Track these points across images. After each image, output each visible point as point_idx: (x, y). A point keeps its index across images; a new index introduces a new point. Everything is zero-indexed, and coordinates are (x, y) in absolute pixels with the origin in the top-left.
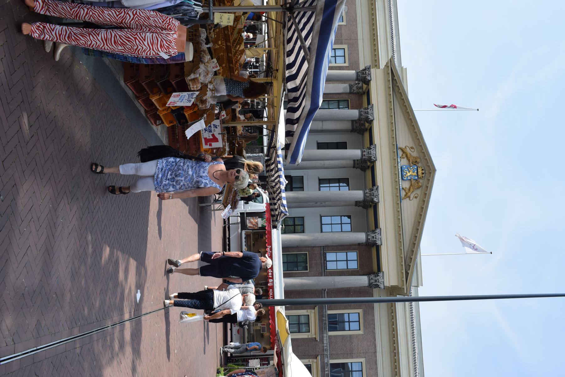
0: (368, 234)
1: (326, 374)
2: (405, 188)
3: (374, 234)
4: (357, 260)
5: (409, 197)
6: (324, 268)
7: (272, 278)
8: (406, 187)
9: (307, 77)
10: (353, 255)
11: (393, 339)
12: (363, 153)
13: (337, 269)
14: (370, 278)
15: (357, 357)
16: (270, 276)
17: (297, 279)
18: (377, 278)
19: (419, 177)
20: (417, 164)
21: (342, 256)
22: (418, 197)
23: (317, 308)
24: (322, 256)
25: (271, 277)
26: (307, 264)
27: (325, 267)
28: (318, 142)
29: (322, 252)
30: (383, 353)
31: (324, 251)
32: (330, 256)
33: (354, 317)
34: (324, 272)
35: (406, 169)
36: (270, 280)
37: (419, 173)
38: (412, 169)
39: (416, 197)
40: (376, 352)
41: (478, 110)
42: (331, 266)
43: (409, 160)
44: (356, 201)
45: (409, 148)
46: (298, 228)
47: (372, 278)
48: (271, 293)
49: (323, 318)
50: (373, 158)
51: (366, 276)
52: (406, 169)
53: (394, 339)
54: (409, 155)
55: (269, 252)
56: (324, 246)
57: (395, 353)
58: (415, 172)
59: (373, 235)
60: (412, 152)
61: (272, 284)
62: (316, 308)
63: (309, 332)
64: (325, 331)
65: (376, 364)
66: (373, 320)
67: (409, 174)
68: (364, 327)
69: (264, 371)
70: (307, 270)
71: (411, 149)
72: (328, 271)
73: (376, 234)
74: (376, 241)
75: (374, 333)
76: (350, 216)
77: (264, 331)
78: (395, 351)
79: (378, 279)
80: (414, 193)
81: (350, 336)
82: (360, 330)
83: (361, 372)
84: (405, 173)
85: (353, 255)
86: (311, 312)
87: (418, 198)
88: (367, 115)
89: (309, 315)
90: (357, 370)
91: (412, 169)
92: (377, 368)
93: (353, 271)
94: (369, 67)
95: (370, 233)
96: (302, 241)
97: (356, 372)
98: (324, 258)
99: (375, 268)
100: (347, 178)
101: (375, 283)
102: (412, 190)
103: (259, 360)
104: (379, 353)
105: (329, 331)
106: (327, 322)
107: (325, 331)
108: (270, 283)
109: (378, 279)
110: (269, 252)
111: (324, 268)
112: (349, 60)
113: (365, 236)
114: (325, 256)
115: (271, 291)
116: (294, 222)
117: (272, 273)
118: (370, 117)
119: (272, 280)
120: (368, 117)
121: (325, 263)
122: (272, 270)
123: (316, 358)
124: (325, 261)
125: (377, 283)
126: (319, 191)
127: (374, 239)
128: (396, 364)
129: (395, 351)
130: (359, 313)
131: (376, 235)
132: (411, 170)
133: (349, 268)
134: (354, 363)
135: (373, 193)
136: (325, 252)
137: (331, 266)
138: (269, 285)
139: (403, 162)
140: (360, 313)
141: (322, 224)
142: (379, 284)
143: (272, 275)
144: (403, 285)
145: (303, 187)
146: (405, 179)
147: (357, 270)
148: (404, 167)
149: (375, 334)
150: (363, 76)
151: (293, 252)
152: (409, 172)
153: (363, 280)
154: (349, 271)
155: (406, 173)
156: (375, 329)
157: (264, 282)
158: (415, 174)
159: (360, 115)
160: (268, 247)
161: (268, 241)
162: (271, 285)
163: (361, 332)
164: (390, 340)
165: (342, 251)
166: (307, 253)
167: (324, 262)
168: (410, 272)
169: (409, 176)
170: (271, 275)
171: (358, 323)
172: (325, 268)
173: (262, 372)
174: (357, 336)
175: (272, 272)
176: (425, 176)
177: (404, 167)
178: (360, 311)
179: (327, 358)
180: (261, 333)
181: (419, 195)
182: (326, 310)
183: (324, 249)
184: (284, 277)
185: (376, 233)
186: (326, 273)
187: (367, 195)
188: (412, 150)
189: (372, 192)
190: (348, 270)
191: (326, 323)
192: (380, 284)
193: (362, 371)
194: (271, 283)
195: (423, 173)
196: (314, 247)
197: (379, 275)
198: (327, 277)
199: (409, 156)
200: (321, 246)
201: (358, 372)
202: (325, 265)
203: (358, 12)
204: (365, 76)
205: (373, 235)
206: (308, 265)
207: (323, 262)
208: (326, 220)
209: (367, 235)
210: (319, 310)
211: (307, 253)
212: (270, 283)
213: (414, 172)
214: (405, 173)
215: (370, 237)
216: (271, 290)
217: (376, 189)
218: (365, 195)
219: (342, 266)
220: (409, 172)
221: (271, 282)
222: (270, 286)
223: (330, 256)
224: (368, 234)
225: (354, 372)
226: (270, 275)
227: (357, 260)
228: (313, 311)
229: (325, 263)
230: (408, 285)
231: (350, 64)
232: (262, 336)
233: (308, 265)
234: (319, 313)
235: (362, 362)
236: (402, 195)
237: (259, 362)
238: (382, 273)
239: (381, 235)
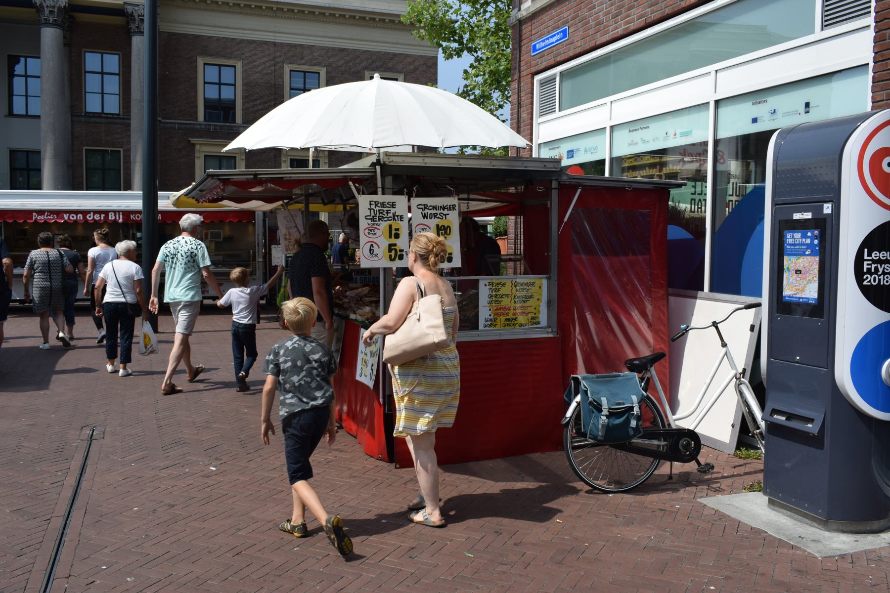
0: (43, 21)
3: (44, 9)
4: (102, 54)
6: (116, 118)
7: (106, 213)
10: (92, 61)
11: (242, 8)
12: (51, 22)
13: (119, 95)
15: (282, 78)
16: (102, 218)
17: (134, 171)
18: (136, 17)
21: (92, 83)
23: (193, 140)
24: (93, 120)
25: (103, 216)
26: (108, 150)
27: (115, 116)
28: (7, 114)
29: (83, 119)
30: (277, 31)
31: (82, 116)
32: (93, 104)
33: (212, 74)
34: (123, 119)
36: (111, 217)
40: (274, 44)
42: (113, 106)
44: (64, 46)
47: (137, 27)
48: (138, 217)
49: (212, 130)
51: (133, 37)
53: (317, 13)
55: (47, 216)
56: (72, 115)
57: (277, 8)
59: (47, 12)
61: (119, 214)
62: (192, 142)
64: (234, 129)
65: (295, 46)
66: (218, 39)
68: (230, 57)
69: (285, 235)
70: (120, 151)
72: (123, 111)
73: (45, 5)
75: (241, 42)
76: (9, 56)
77: (217, 235)
78: (275, 9)
79: (139, 16)
81: (245, 85)
82: (235, 67)
83: (307, 74)
85: (92, 61)
86: (199, 151)
89: (205, 156)
90: (303, 80)
92: (302, 46)
93: (123, 63)
95: (43, 18)
96: (56, 156)
97: (303, 83)
98: (96, 117)
99: (118, 20)
100: (8, 59)
103: (273, 246)
104: (277, 38)
105: (234, 121)
106: (218, 124)
107: (234, 129)
108: (117, 219)
109: (139, 16)
110: (47, 216)
111: (116, 118)
113: (48, 28)
114: (91, 115)
115: (135, 217)
116: (21, 170)
117: (96, 212)
119: (110, 214)
121: (106, 116)
122: (88, 212)
123: (193, 144)
124: (103, 115)
126: (42, 118)
127: (56, 10)
128: (377, 20)
129: (275, 9)
130: (205, 64)
131: (47, 6)
133: (117, 72)
134: (292, 85)
136: (83, 114)
137: (113, 106)
138: (121, 221)
140: (205, 62)
141: (27, 116)
143: (76, 212)
145: (26, 151)
147: (86, 50)
149: (243, 40)
151: (83, 175)
153: (140, 44)
154: (123, 71)
156: (234, 39)
157: (123, 232)
159: (47, 23)
160: (36, 218)
161: (20, 219)
162: (121, 216)
163: (239, 65)
164: (357, 25)
165: (82, 80)
166: (86, 149)
167: (105, 117)
170: (98, 215)
171: (222, 67)
172: (117, 116)
173: (286, 239)
174: (245, 73)
175: (92, 213)
178: (200, 62)
180: (222, 240)
182: (196, 122)
183: (78, 116)
184: (40, 189)
186: (125, 117)
190: (121, 75)
191: (221, 126)
193: (305, 72)
194: (117, 216)
196: (73, 135)
197: (130, 11)
198: (132, 114)
200: (72, 121)
201: (307, 80)
202: (111, 116)
203: (332, 43)
205: (47, 12)
206: (109, 149)
207: (103, 120)
208: (19, 107)
209: (47, 24)
210: (197, 137)
211: (86, 149)
212: (117, 219)
215: (51, 19)
216: (132, 217)
219: (113, 85)
221: (115, 216)
222: (123, 219)
223: (93, 104)
224: (43, 21)
225: (306, 86)
226: (100, 217)
227: (102, 54)
228: (197, 147)
229: (106, 116)
232: (229, 239)
233: (109, 149)
234: (201, 137)
235: (291, 71)
237: (276, 246)
238: (126, 6)
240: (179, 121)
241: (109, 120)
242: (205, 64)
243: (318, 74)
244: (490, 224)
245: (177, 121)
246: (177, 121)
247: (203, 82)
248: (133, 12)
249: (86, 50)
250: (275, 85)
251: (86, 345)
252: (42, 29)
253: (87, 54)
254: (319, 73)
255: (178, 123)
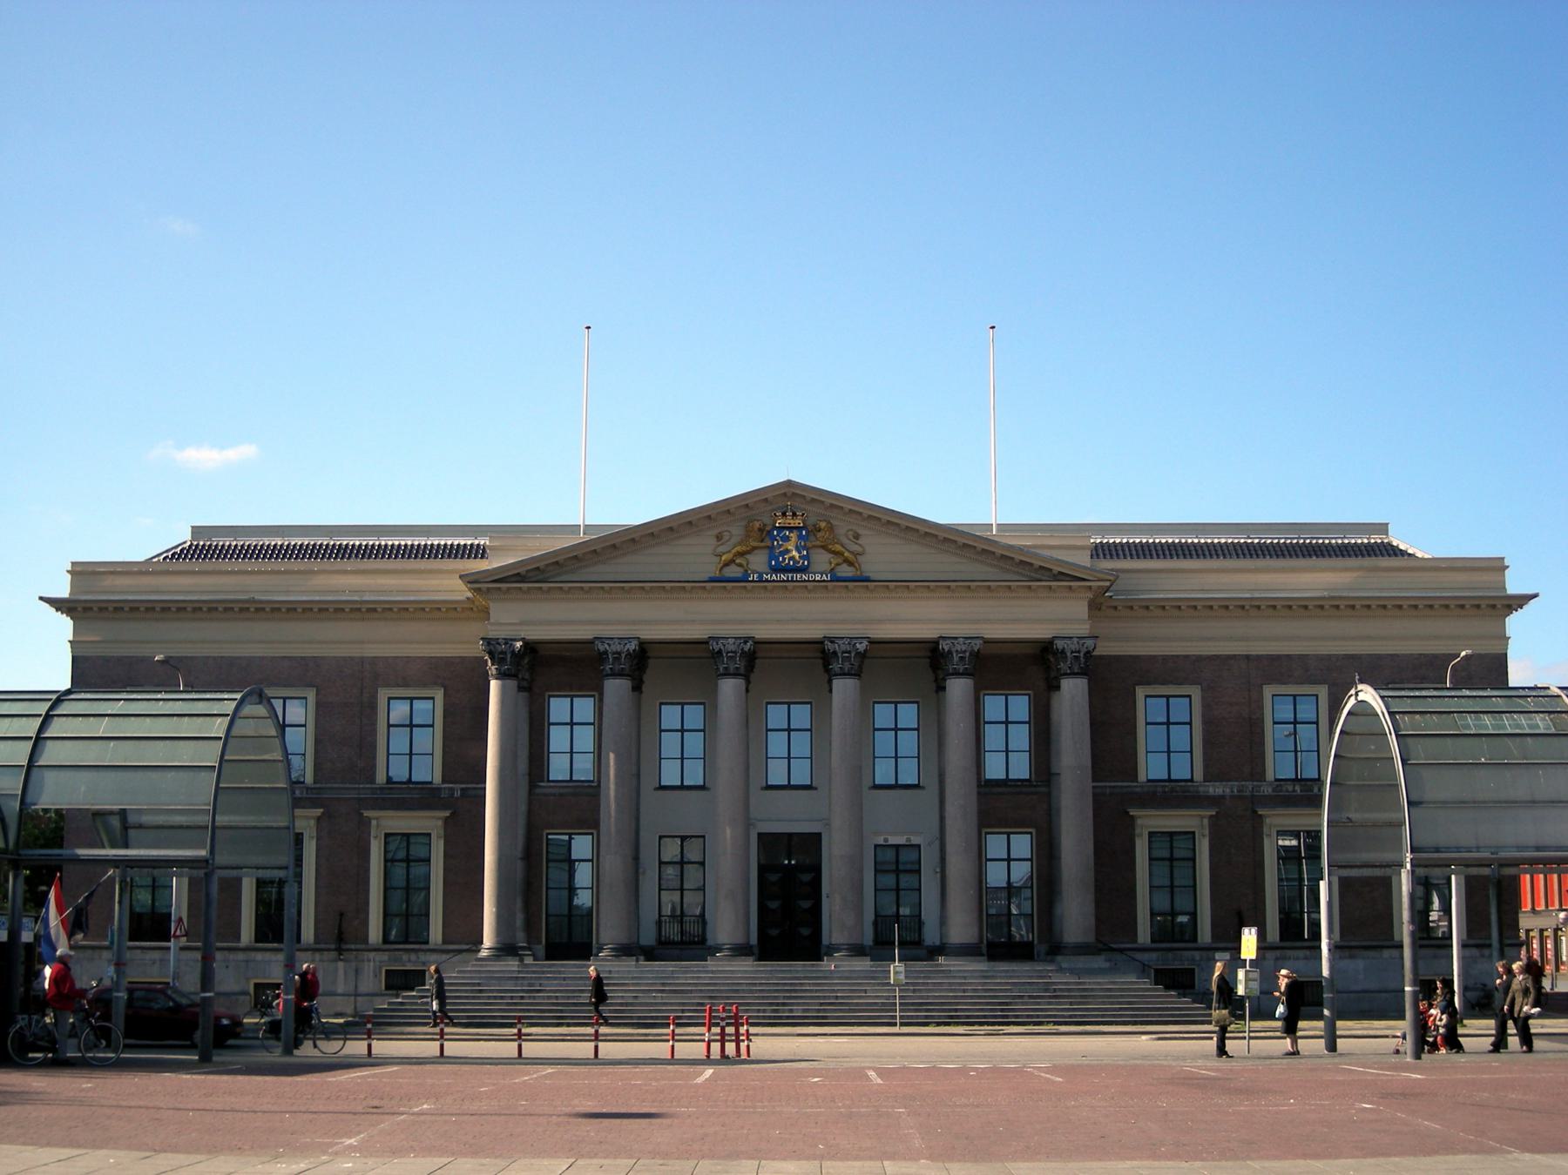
1: (1301, 791)
2: (831, 563)
5: (856, 554)
8: (827, 561)
9: (279, 721)
14: (1069, 671)
18: (1068, 654)
19: (802, 525)
20: (768, 528)
22: (856, 532)
35: (781, 559)
37: (792, 525)
38: (780, 543)
39: (857, 536)
41: (588, 328)
43: (755, 548)
45: (719, 546)
46: (890, 855)
50: (747, 647)
52: (781, 559)
54: (738, 549)
58: (787, 533)
59: (956, 659)
60: (730, 539)
63: (1193, 833)
65: (1278, 658)
66: (1165, 659)
67: (795, 553)
71: (180, 548)
73: (953, 650)
74: (973, 650)
80: (845, 541)
82: (433, 698)
84: (791, 563)
85: (558, 708)
87: (860, 531)
88: (623, 655)
89: (1150, 833)
90: (1292, 707)
91: (780, 543)
94: (486, 643)
101: (1082, 660)
102: (838, 548)
109: (1072, 652)
112: (424, 685)
114: (1019, 783)
118: (633, 646)
120: (629, 654)
121: (1013, 783)
125: (1082, 655)
131: (957, 651)
132: (782, 545)
135: (843, 652)
139: (758, 561)
142: (1084, 650)
144: (1090, 587)
146: (806, 563)
148: (773, 563)
150: (508, 660)
152: (788, 551)
155: (790, 559)
158: (794, 536)
168: (1057, 569)
169: (800, 553)
174: (1206, 706)
176: (801, 510)
177: (773, 563)
178: (1140, 692)
179: (1260, 787)
181: (850, 527)
182: (1136, 784)
185: (950, 652)
187: (846, 669)
188: (726, 536)
189: (840, 655)
192: (1085, 646)
195: (794, 514)
197: (1060, 647)
199: (744, 548)
201: (1298, 707)
204: (509, 656)
213: (788, 537)
214: (791, 563)
217: (832, 642)
218: (848, 674)
219: (1021, 737)
220: (788, 551)
225: (1298, 716)
228: (1139, 822)
230: (1091, 575)
231: (434, 684)
235: (1273, 695)
236: (850, 575)
239: (956, 638)
240: (1113, 784)
241: (1018, 790)
242: (1147, 696)
243: (1188, 699)
244: (374, 819)
245: (1108, 784)
246: (1108, 784)
247: (1320, 724)
248: (1064, 648)
249: (551, 693)
250: (1250, 719)
251: (629, 1111)
252: (606, 682)
253: (551, 699)
254: (1317, 696)
255: (1110, 787)
